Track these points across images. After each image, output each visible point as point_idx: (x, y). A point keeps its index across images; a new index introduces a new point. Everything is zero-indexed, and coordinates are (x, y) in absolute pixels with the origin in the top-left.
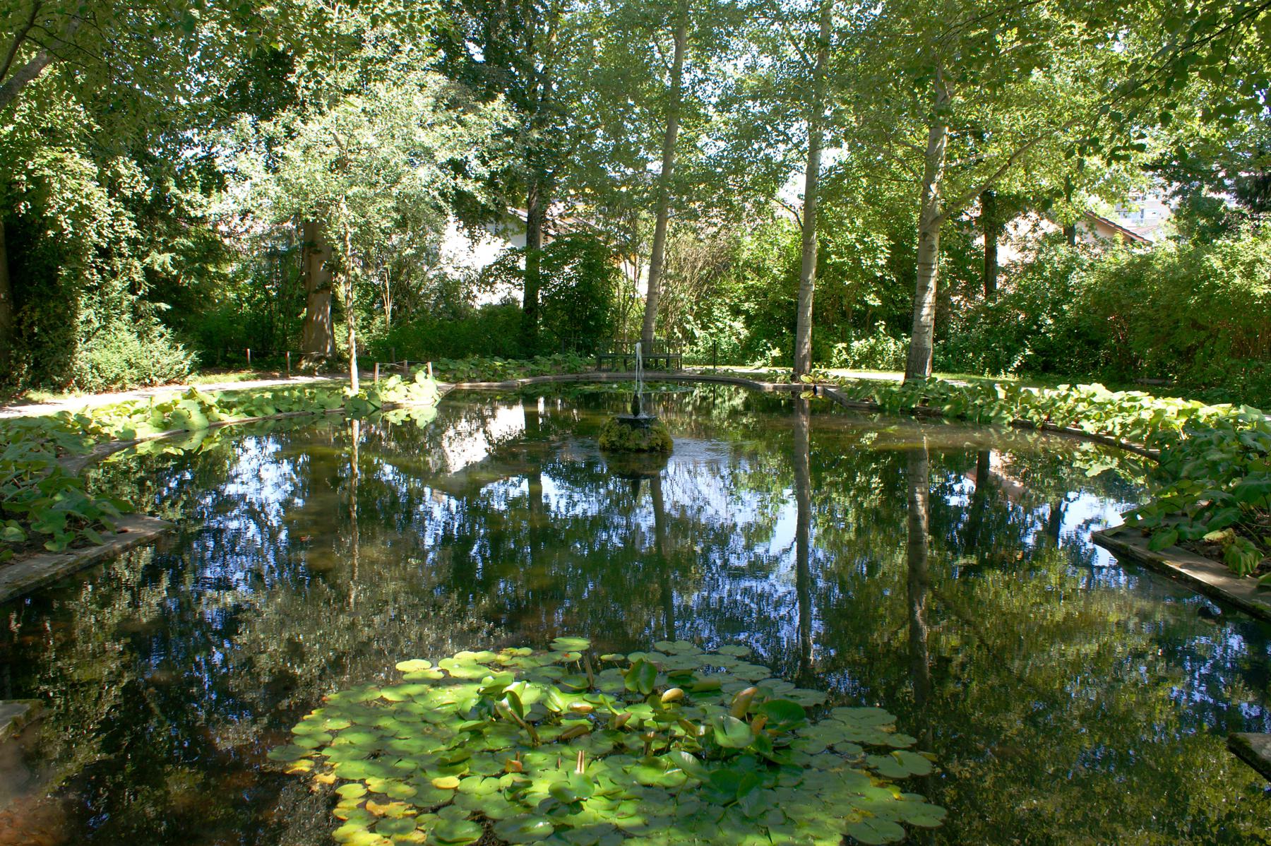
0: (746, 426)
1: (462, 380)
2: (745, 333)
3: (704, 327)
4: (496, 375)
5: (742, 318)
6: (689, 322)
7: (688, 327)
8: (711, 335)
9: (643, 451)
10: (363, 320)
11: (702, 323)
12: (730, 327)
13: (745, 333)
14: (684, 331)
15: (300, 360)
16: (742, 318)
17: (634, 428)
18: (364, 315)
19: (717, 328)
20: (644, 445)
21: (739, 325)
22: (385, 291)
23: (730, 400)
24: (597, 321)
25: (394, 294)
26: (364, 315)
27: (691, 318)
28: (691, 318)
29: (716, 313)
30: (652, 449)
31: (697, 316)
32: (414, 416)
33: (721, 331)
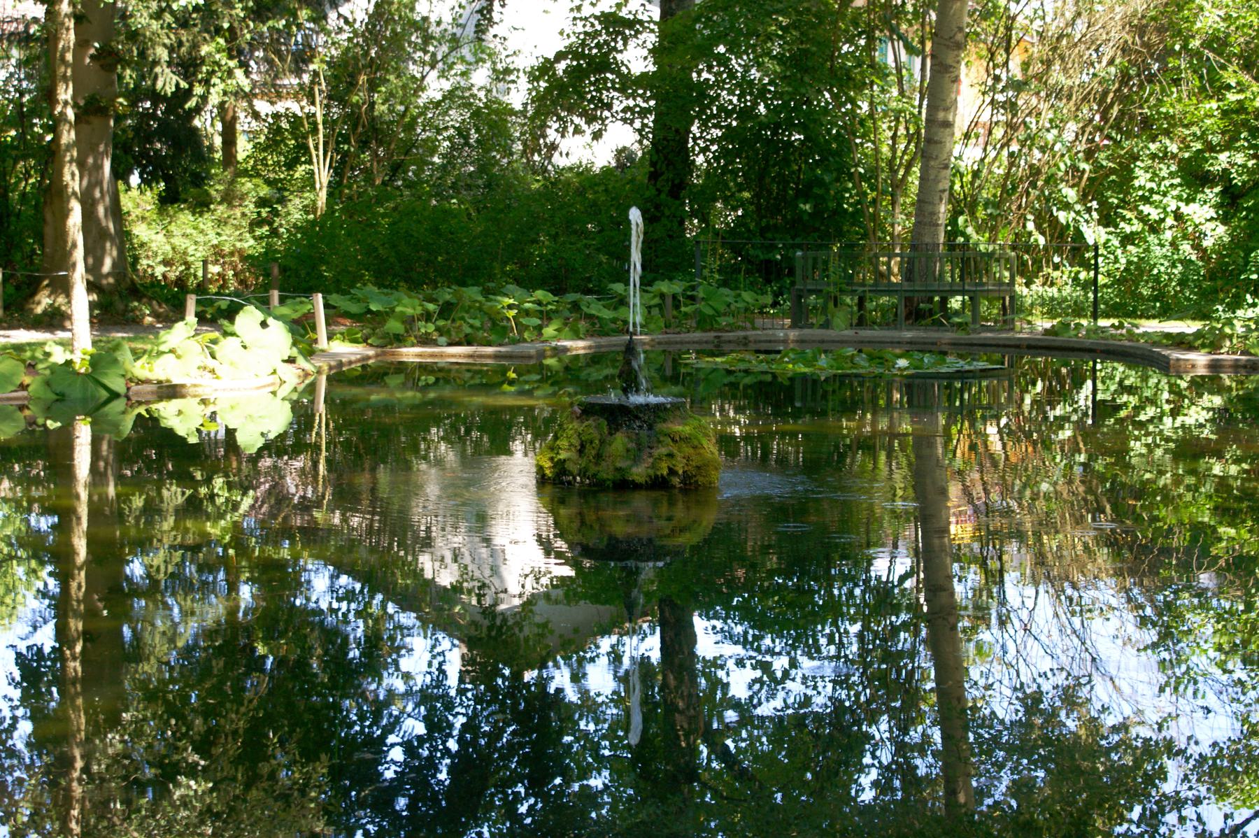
0: (1223, 483)
1: (399, 340)
2: (1214, 234)
3: (1108, 219)
4: (497, 328)
5: (1212, 194)
6: (1067, 206)
7: (1063, 217)
8: (1127, 240)
9: (637, 487)
10: (261, 203)
11: (1103, 204)
12: (1178, 216)
13: (1214, 234)
14: (1058, 233)
15: (34, 293)
16: (1212, 194)
17: (614, 427)
18: (265, 191)
19: (1143, 219)
20: (639, 473)
21: (1201, 212)
22: (315, 131)
23: (1174, 413)
24: (819, 202)
25: (335, 141)
26: (265, 191)
27: (1071, 194)
28: (1071, 194)
29: (1142, 179)
30: (659, 484)
31: (1092, 190)
32: (228, 419)
33: (1155, 228)
